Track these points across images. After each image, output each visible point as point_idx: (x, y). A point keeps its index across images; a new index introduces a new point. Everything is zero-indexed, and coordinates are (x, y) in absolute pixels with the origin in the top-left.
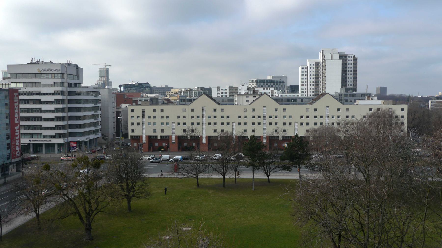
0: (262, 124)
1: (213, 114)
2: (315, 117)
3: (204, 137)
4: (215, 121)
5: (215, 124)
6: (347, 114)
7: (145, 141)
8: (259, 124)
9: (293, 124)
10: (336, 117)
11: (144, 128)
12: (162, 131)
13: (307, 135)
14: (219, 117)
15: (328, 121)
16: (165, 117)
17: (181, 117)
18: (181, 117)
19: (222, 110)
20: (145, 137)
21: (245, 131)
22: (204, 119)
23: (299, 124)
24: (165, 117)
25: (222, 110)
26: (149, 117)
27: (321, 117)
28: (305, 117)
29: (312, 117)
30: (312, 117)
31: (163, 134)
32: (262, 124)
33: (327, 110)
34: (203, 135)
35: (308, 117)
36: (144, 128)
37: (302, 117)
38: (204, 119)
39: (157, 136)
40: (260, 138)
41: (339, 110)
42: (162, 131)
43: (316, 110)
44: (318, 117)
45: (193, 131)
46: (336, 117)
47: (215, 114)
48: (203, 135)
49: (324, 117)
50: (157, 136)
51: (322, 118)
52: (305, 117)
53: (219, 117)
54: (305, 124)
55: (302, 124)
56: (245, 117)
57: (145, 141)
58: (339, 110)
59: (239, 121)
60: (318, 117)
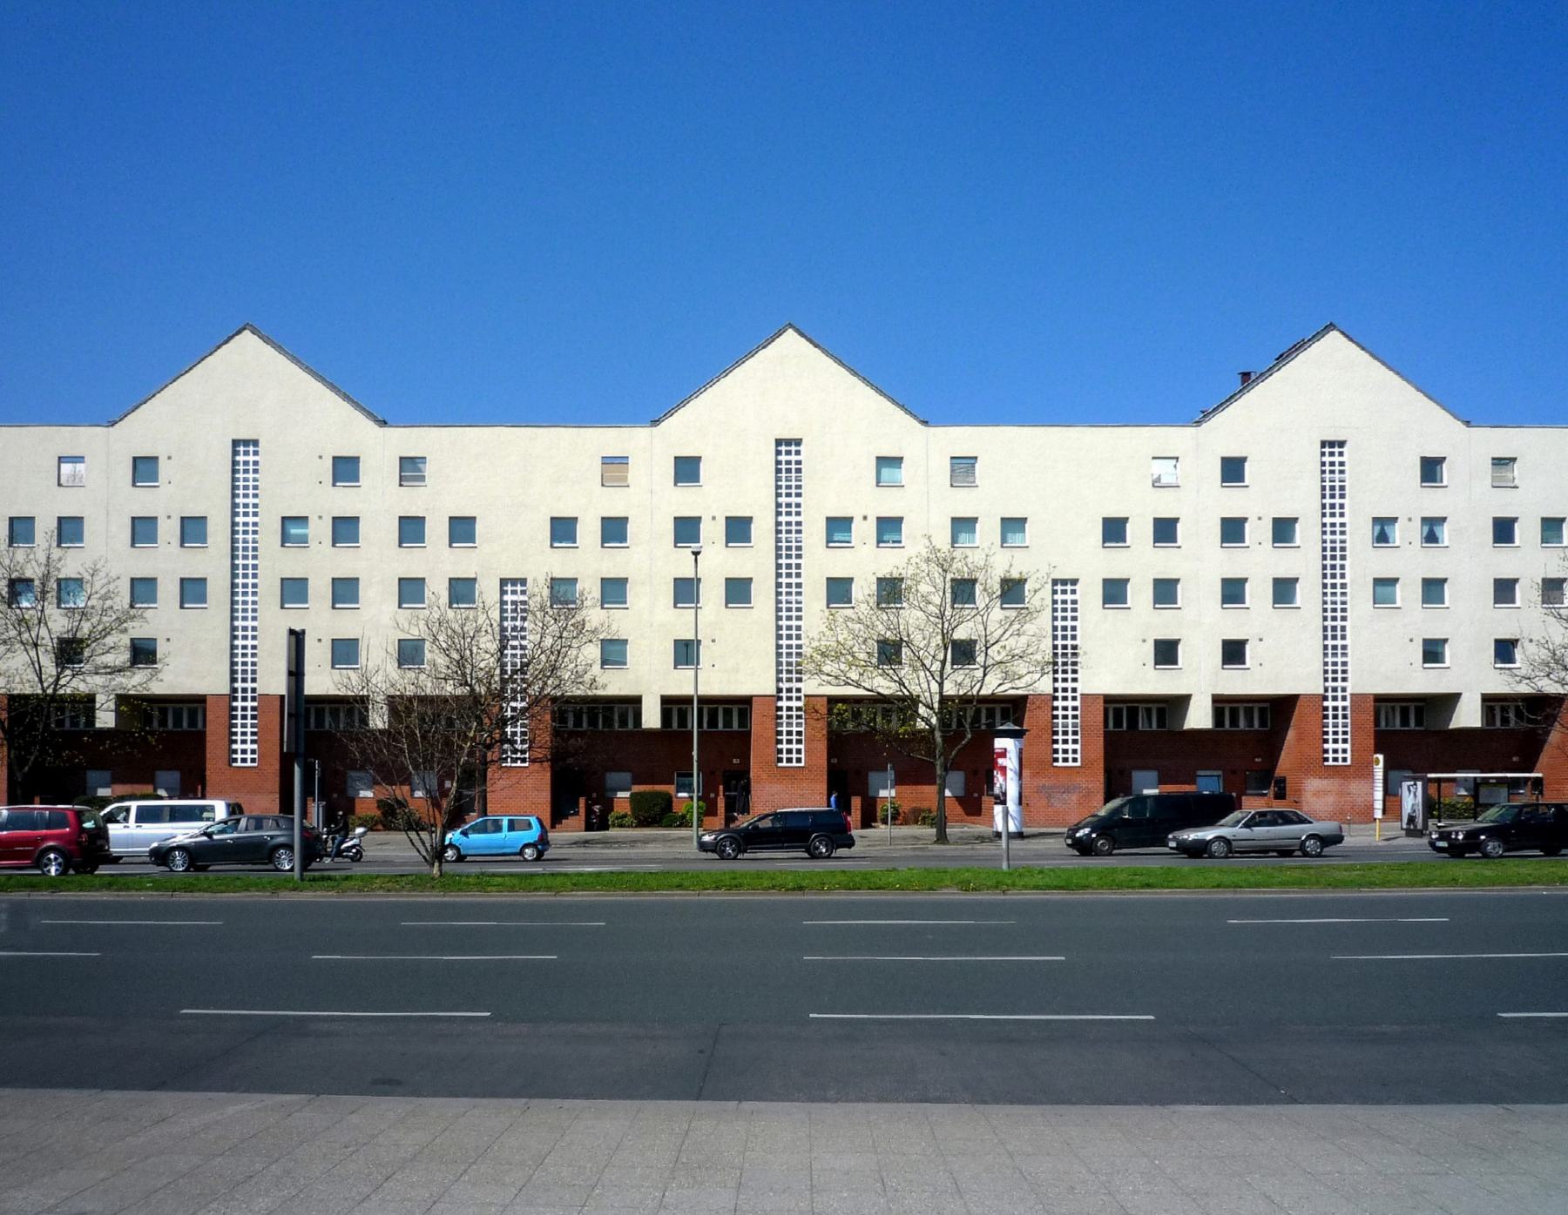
0: (763, 594)
1: (1417, 502)
2: (1504, 530)
3: (794, 704)
4: (345, 562)
5: (1165, 591)
6: (964, 503)
7: (249, 746)
8: (1284, 590)
9: (1038, 596)
10: (1407, 533)
11: (1333, 632)
12: (1234, 652)
13: (114, 700)
14: (379, 530)
15: (794, 561)
16: (437, 530)
17: (589, 531)
18: (589, 531)
19: (410, 469)
20: (249, 704)
21: (889, 652)
22: (787, 552)
23: (1090, 595)
24: (437, 530)
25: (410, 469)
26: (1382, 530)
27: (1283, 530)
28: (1140, 531)
29: (1199, 532)
30: (1199, 532)
31: (1239, 683)
32: (763, 594)
33: (1327, 468)
34: (1056, 690)
35: (1165, 530)
36: (1333, 632)
37: (1114, 530)
38: (787, 552)
39: (636, 701)
40: (193, 722)
41: (1431, 469)
42: (1234, 652)
43: (1233, 470)
44: (1258, 532)
45: (963, 652)
46: (1407, 533)
47: (344, 501)
48: (1056, 690)
49: (1307, 534)
50: (636, 701)
51: (623, 538)
52: (1140, 531)
53: (379, 530)
54: (1140, 594)
55: (1114, 592)
56: (614, 530)
57: (249, 746)
58: (1431, 469)
59: (1115, 563)
60: (1258, 532)
